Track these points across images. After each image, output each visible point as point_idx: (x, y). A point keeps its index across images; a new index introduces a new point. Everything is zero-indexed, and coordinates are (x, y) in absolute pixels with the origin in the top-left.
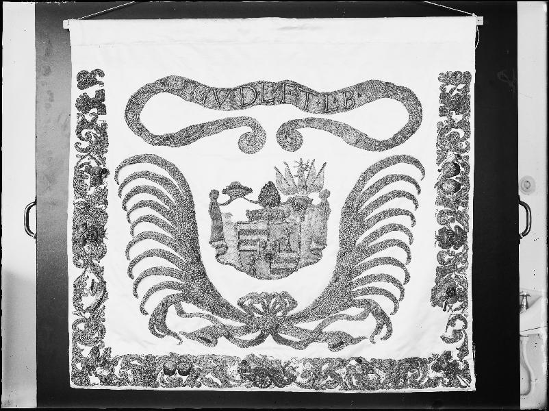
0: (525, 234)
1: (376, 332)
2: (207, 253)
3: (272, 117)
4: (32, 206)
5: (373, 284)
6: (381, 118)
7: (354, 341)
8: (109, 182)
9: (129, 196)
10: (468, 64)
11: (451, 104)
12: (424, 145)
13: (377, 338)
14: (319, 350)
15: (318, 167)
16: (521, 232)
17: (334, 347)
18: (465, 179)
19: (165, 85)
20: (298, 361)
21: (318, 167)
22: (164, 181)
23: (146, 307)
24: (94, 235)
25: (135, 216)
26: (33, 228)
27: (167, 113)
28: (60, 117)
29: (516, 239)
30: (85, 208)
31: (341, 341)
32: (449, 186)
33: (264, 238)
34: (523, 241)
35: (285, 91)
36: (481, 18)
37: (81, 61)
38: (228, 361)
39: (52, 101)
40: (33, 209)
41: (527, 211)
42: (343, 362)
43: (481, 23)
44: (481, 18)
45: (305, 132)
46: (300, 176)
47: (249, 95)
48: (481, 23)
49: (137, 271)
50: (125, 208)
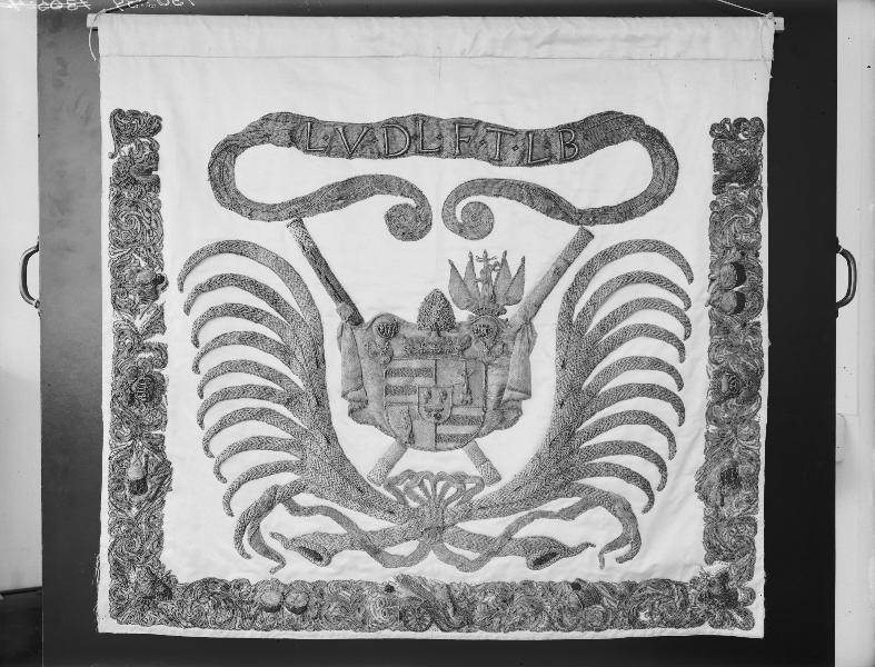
0: (845, 302)
1: (612, 546)
2: (338, 407)
3: (436, 176)
4: (34, 252)
5: (595, 285)
6: (617, 171)
7: (568, 552)
8: (171, 299)
9: (211, 376)
10: (755, 105)
11: (732, 173)
12: (686, 219)
13: (610, 557)
14: (511, 569)
15: (513, 268)
16: (839, 298)
17: (539, 563)
18: (756, 289)
19: (259, 133)
20: (478, 570)
21: (513, 268)
22: (265, 393)
23: (224, 470)
24: (146, 389)
25: (220, 444)
26: (34, 291)
27: (273, 173)
28: (77, 104)
29: (829, 309)
30: (133, 342)
31: (547, 553)
32: (729, 301)
33: (429, 382)
34: (841, 310)
35: (467, 137)
36: (781, 21)
37: (117, 91)
38: (365, 574)
39: (65, 75)
40: (35, 261)
41: (848, 260)
42: (550, 588)
43: (781, 27)
44: (781, 21)
45: (499, 206)
46: (487, 281)
47: (401, 140)
48: (781, 27)
49: (206, 336)
50: (196, 368)
